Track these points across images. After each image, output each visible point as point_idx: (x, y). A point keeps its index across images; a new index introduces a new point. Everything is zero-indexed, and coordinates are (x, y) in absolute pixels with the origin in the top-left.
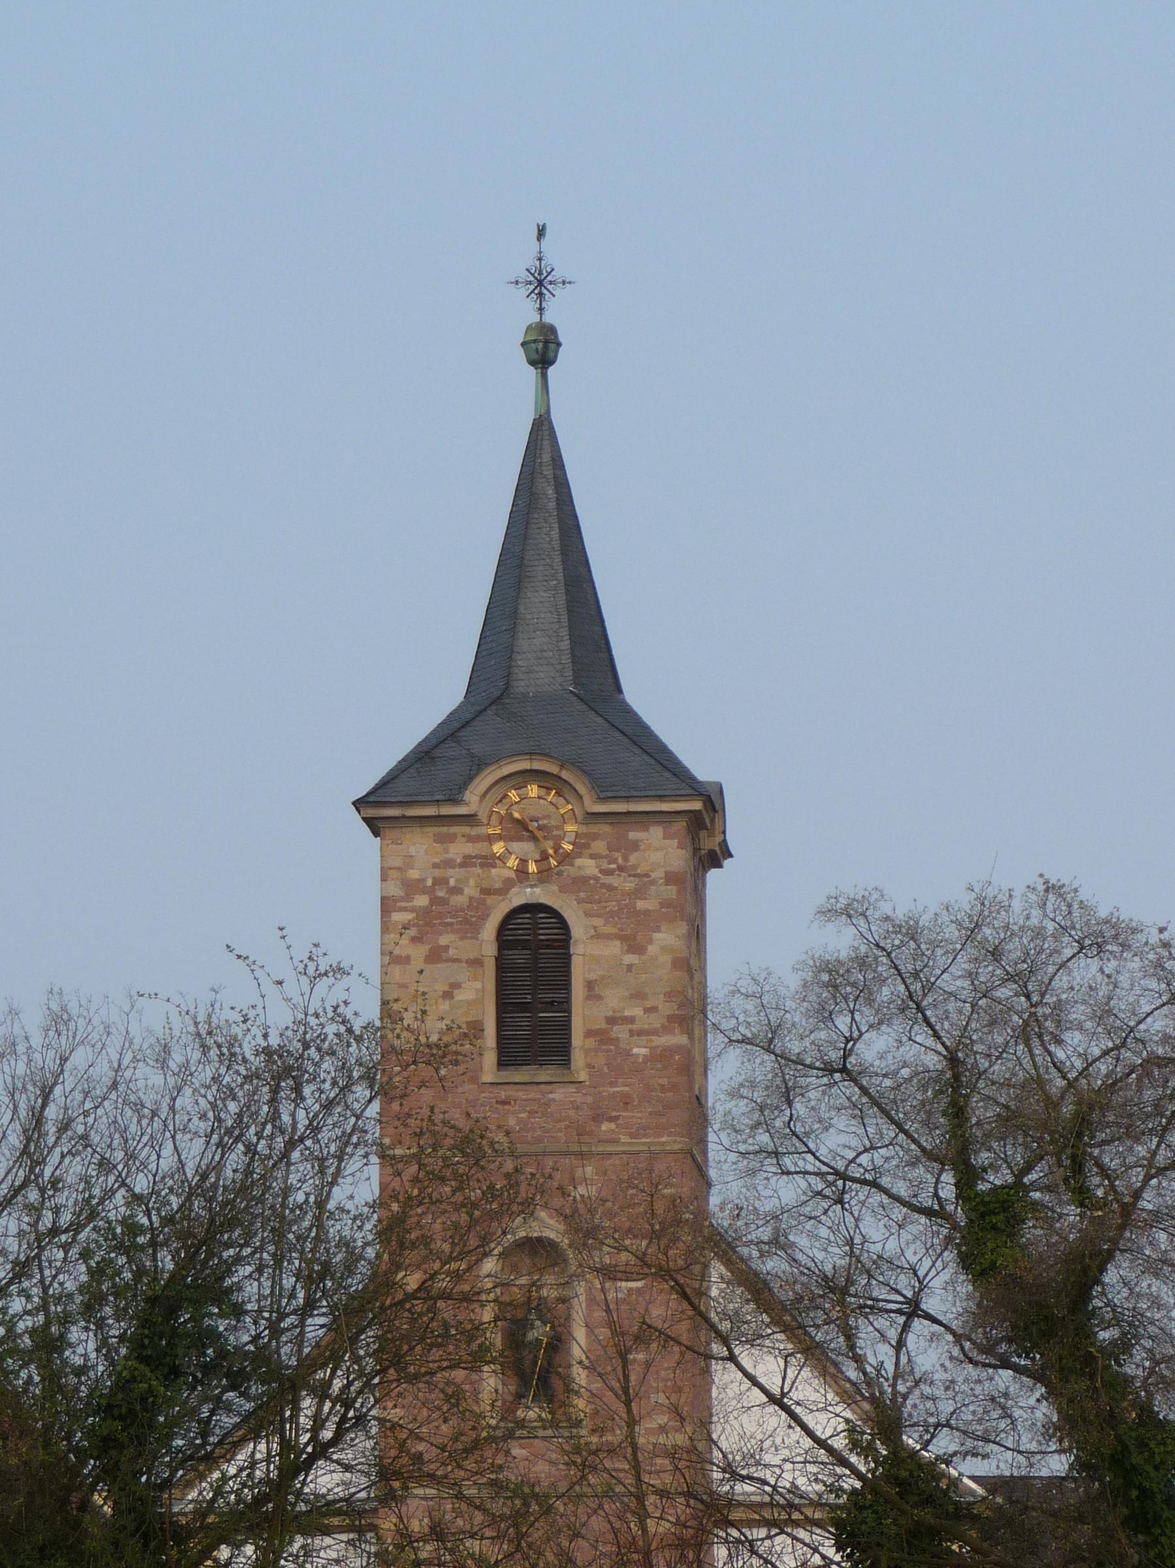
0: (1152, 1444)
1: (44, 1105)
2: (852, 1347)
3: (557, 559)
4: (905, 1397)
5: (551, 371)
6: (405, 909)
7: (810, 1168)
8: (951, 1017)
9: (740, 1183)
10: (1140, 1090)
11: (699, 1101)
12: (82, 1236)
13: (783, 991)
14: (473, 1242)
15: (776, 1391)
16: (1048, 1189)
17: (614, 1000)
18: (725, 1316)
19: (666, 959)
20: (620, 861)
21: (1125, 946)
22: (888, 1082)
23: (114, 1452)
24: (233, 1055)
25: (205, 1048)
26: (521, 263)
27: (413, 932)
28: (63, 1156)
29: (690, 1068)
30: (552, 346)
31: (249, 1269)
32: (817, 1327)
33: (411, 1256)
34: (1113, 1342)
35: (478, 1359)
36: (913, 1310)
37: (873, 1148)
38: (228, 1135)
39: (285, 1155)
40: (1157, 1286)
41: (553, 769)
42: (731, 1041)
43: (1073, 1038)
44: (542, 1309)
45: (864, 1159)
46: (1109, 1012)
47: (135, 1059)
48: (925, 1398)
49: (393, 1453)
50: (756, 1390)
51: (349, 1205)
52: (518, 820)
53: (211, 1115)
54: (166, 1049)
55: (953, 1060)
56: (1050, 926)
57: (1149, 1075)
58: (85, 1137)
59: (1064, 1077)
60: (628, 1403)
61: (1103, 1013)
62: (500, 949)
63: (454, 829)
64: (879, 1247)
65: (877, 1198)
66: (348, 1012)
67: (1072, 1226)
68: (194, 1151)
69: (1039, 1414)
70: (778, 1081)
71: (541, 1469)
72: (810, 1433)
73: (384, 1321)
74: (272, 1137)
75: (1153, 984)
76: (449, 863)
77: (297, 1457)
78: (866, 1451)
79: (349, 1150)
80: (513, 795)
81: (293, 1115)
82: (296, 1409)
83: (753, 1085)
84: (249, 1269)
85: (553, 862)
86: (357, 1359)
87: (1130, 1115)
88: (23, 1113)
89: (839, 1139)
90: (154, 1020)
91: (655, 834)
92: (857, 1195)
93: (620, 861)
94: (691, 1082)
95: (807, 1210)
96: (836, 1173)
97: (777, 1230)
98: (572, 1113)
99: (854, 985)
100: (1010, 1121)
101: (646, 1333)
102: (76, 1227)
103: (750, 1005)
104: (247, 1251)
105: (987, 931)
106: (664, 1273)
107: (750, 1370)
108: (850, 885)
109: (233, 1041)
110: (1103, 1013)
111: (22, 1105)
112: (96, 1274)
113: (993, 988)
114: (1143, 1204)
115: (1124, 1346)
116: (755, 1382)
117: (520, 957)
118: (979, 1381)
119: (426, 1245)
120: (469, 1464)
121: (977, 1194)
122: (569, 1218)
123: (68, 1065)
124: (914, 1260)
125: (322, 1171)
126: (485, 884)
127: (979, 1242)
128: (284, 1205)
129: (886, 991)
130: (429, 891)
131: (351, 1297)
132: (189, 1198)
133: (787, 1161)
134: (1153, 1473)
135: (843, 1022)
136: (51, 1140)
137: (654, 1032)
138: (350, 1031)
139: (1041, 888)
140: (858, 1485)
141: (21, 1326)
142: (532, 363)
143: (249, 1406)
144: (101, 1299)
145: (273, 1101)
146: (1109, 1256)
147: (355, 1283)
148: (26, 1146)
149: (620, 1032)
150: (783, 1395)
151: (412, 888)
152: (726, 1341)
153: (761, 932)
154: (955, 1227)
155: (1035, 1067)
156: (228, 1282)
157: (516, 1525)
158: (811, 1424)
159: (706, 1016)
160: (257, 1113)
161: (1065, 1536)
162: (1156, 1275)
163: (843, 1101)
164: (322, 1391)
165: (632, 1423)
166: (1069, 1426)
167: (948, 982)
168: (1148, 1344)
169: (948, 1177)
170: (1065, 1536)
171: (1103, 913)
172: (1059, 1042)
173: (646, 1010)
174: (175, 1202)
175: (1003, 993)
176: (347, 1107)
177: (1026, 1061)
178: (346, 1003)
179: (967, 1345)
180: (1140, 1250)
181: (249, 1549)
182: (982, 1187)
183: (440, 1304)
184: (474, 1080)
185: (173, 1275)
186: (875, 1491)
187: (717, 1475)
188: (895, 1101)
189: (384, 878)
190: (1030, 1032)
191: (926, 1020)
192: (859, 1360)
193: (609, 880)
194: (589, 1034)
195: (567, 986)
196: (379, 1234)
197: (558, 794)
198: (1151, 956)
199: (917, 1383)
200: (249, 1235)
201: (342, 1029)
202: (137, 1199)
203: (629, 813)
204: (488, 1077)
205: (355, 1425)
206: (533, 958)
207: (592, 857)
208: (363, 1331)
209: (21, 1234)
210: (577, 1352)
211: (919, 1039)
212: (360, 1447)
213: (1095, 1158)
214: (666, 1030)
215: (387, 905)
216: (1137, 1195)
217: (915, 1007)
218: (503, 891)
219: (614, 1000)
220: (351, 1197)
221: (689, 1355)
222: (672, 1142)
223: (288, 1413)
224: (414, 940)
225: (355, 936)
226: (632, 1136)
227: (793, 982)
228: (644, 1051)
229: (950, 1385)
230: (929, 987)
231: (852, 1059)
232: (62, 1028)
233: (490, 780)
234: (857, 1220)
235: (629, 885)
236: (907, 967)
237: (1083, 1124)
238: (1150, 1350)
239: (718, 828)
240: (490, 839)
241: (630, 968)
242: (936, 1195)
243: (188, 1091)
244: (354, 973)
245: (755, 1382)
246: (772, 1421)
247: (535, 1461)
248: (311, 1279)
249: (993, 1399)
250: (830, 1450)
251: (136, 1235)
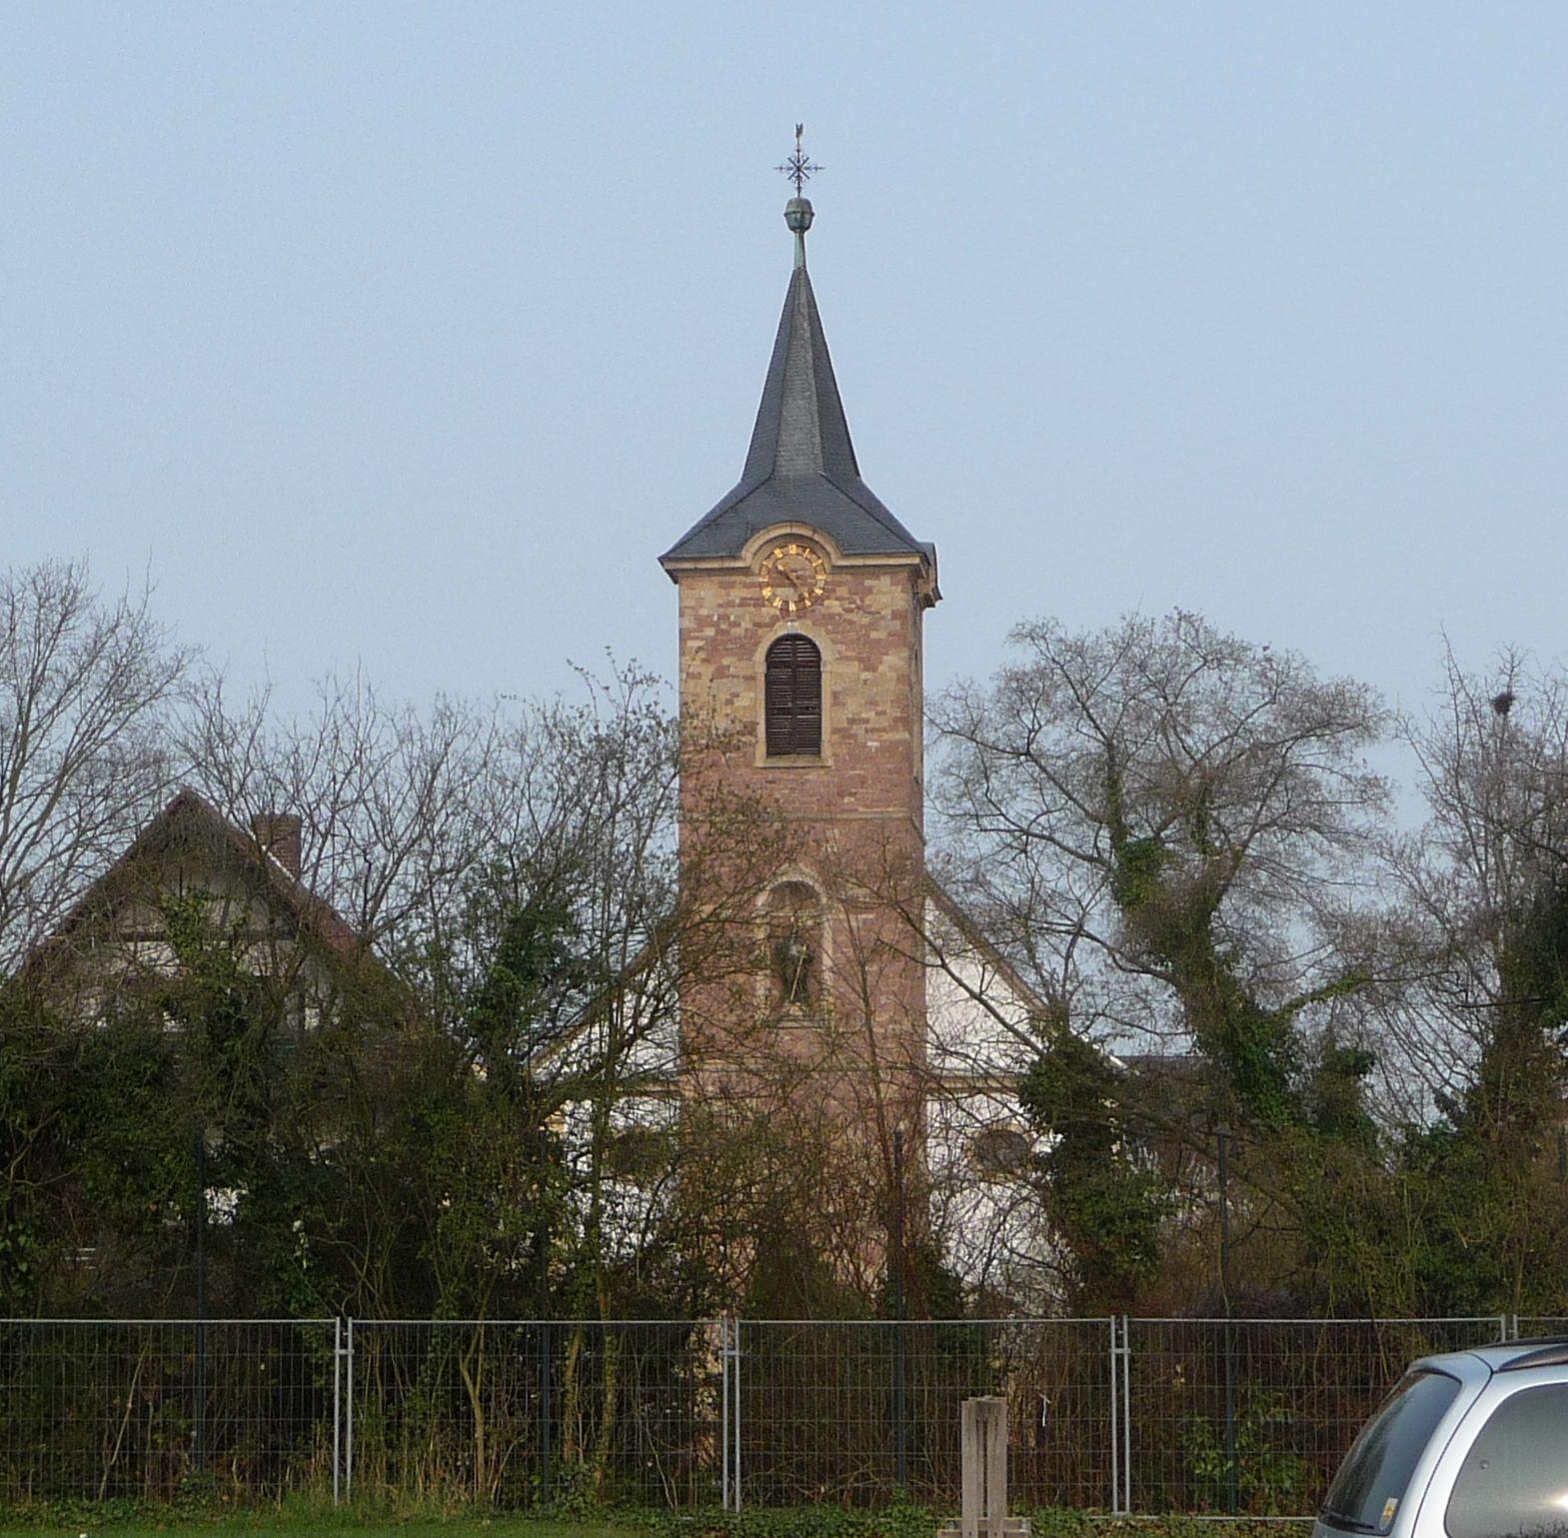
0: (1254, 1028)
1: (433, 778)
2: (1033, 958)
3: (811, 373)
4: (1072, 994)
5: (806, 234)
6: (697, 638)
7: (1002, 827)
8: (1108, 713)
9: (950, 838)
10: (1248, 766)
11: (918, 781)
12: (462, 875)
13: (982, 694)
14: (751, 881)
15: (977, 990)
16: (1177, 841)
17: (853, 705)
18: (937, 934)
19: (894, 675)
21: (1238, 661)
22: (1060, 762)
23: (487, 1032)
24: (573, 741)
25: (552, 737)
26: (786, 153)
27: (702, 655)
28: (447, 815)
29: (910, 757)
30: (807, 216)
31: (585, 900)
32: (1007, 944)
33: (704, 892)
34: (1225, 954)
35: (756, 966)
36: (1078, 931)
37: (1049, 811)
38: (569, 802)
39: (612, 816)
40: (1258, 911)
41: (809, 533)
42: (943, 732)
43: (1199, 729)
44: (797, 934)
45: (1042, 820)
46: (1226, 710)
47: (500, 745)
48: (1086, 994)
49: (693, 1034)
50: (961, 989)
51: (659, 853)
52: (781, 572)
53: (556, 786)
54: (523, 738)
55: (1109, 746)
56: (1183, 646)
57: (1255, 756)
58: (465, 802)
59: (1192, 758)
60: (866, 1001)
61: (1221, 711)
62: (768, 668)
63: (733, 578)
64: (1053, 884)
65: (1053, 848)
66: (658, 710)
67: (1197, 867)
68: (544, 814)
69: (1170, 1006)
70: (979, 762)
71: (800, 1048)
72: (1002, 1021)
73: (686, 940)
74: (601, 803)
75: (1259, 689)
76: (730, 604)
77: (623, 1036)
78: (1041, 1034)
79: (659, 812)
80: (778, 553)
81: (617, 787)
82: (621, 1003)
83: (960, 765)
84: (585, 900)
85: (808, 603)
86: (665, 966)
87: (1241, 787)
88: (417, 784)
89: (1024, 805)
90: (513, 717)
91: (886, 580)
92: (1037, 847)
94: (911, 766)
95: (999, 858)
96: (1021, 830)
97: (978, 872)
98: (822, 790)
99: (1036, 690)
100: (1151, 791)
101: (879, 948)
102: (458, 869)
103: (958, 706)
104: (583, 887)
105: (1136, 650)
106: (894, 904)
107: (957, 974)
108: (1033, 617)
109: (573, 732)
110: (1221, 711)
111: (418, 778)
112: (474, 903)
113: (1141, 692)
114: (1249, 851)
115: (1234, 956)
116: (961, 984)
117: (784, 674)
118: (1126, 982)
119: (717, 883)
120: (749, 1043)
121: (1127, 845)
122: (823, 865)
123: (450, 750)
124: (1078, 893)
125: (639, 828)
126: (757, 620)
127: (1129, 880)
128: (611, 853)
129: (1059, 694)
130: (716, 625)
131: (663, 921)
132: (541, 847)
133: (985, 822)
134: (1254, 1048)
135: (1027, 718)
136: (439, 804)
137: (884, 730)
138: (659, 724)
139: (1176, 617)
140: (1036, 1058)
141: (418, 940)
142: (793, 229)
143: (586, 1000)
144: (478, 921)
145: (603, 776)
146: (1225, 890)
147: (664, 911)
148: (421, 809)
149: (858, 730)
150: (981, 992)
151: (702, 622)
152: (939, 953)
153: (965, 651)
154: (1110, 869)
155: (1171, 752)
156: (570, 909)
157: (783, 1087)
158: (1002, 1014)
159: (922, 713)
160: (591, 785)
161: (1190, 1094)
162: (1259, 904)
163: (1027, 777)
164: (640, 991)
165: (869, 1014)
166: (1194, 1015)
167: (1106, 688)
168: (1252, 954)
169: (1105, 833)
170: (1190, 1094)
171: (1222, 637)
172: (1189, 732)
173: (877, 714)
174: (530, 851)
175: (1147, 695)
176: (657, 780)
177: (1164, 747)
178: (656, 703)
179: (1118, 956)
180: (1247, 884)
181: (587, 1104)
182: (1129, 840)
183: (727, 925)
184: (748, 765)
185: (529, 904)
186: (1049, 1063)
187: (930, 1051)
188: (1066, 777)
189: (681, 615)
190: (1167, 725)
191: (1090, 716)
192: (1038, 968)
193: (850, 616)
194: (835, 731)
195: (819, 696)
196: (681, 875)
197: (812, 552)
198: (1257, 668)
199: (1081, 984)
200: (585, 875)
201: (653, 723)
202: (504, 847)
203: (864, 566)
204: (759, 764)
205: (665, 1014)
206: (793, 675)
208: (670, 945)
209: (417, 873)
210: (827, 962)
211: (1084, 730)
212: (669, 1029)
214: (893, 728)
215: (684, 636)
216: (1245, 845)
217: (1081, 707)
218: (771, 625)
219: (853, 705)
220: (661, 847)
221: (911, 964)
222: (896, 812)
223: (615, 1005)
224: (704, 661)
225: (664, 658)
226: (866, 806)
227: (989, 688)
228: (876, 744)
229: (1105, 985)
230: (1091, 692)
231: (1034, 746)
232: (446, 721)
233: (756, 546)
234: (1037, 865)
235: (865, 620)
236: (1075, 677)
237: (1205, 793)
238: (1253, 959)
239: (932, 577)
240: (761, 586)
241: (865, 681)
242: (1096, 846)
243: (539, 768)
244: (662, 681)
245: (961, 984)
246: (971, 1016)
247: (798, 1042)
248: (630, 908)
249: (1137, 995)
250: (1016, 1033)
251: (502, 874)
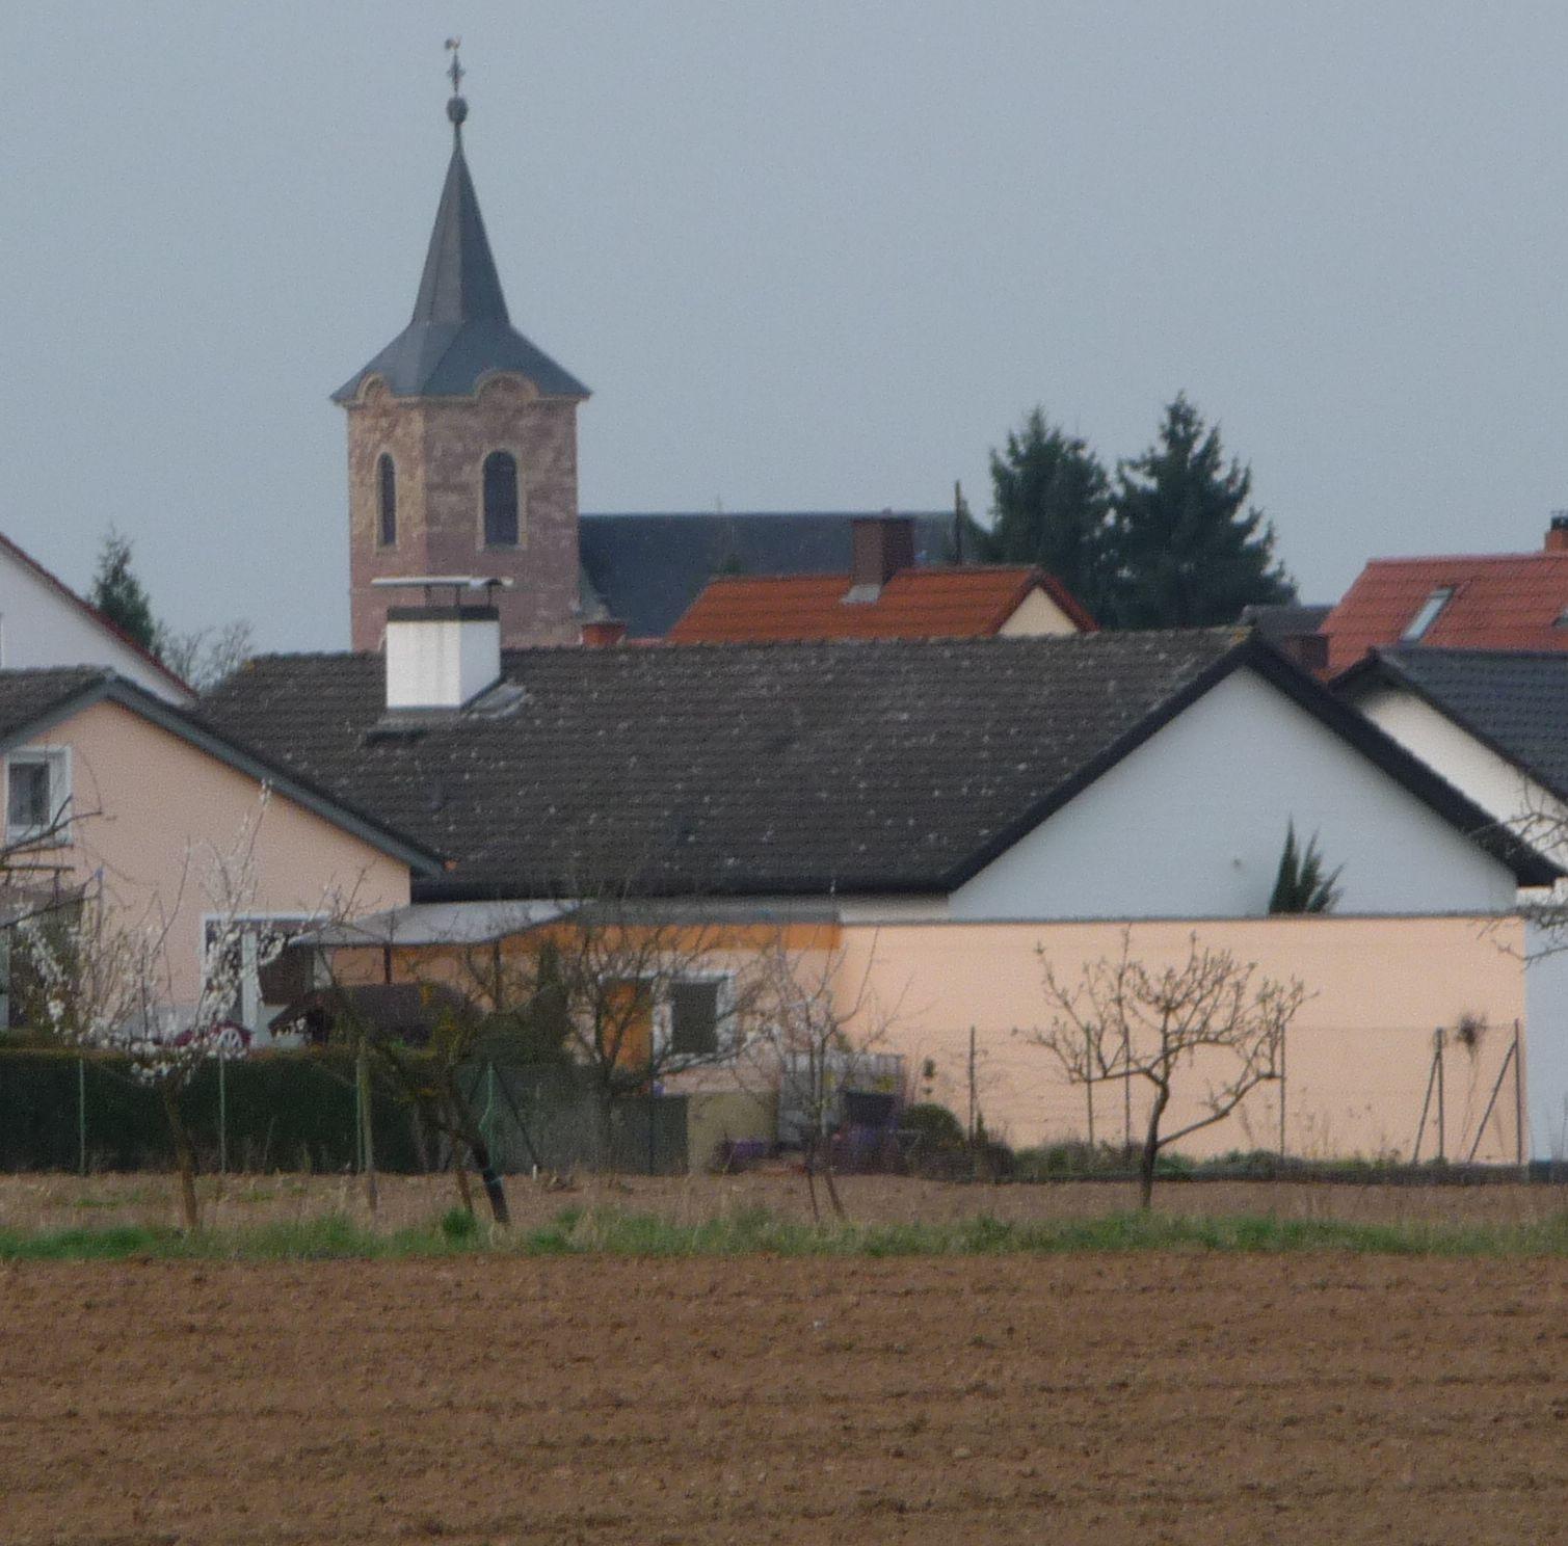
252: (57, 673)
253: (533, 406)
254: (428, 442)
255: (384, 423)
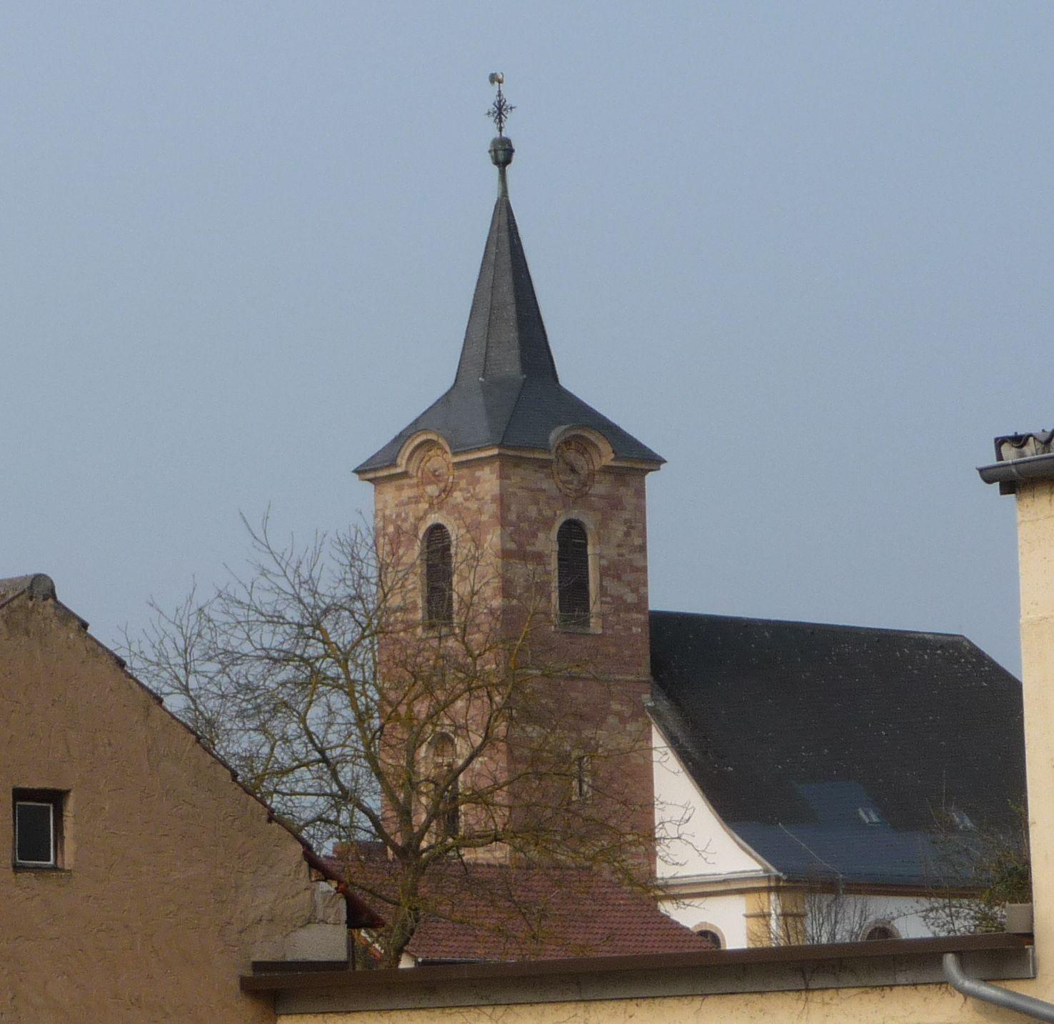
20: (472, 491)
93: (472, 491)
203: (467, 461)
207: (460, 490)
213: (435, 791)
233: (407, 454)
252: (656, 455)
253: (607, 470)
254: (503, 501)
255: (432, 490)
